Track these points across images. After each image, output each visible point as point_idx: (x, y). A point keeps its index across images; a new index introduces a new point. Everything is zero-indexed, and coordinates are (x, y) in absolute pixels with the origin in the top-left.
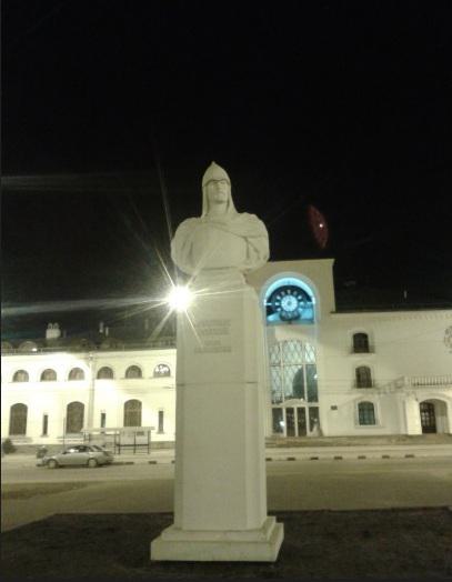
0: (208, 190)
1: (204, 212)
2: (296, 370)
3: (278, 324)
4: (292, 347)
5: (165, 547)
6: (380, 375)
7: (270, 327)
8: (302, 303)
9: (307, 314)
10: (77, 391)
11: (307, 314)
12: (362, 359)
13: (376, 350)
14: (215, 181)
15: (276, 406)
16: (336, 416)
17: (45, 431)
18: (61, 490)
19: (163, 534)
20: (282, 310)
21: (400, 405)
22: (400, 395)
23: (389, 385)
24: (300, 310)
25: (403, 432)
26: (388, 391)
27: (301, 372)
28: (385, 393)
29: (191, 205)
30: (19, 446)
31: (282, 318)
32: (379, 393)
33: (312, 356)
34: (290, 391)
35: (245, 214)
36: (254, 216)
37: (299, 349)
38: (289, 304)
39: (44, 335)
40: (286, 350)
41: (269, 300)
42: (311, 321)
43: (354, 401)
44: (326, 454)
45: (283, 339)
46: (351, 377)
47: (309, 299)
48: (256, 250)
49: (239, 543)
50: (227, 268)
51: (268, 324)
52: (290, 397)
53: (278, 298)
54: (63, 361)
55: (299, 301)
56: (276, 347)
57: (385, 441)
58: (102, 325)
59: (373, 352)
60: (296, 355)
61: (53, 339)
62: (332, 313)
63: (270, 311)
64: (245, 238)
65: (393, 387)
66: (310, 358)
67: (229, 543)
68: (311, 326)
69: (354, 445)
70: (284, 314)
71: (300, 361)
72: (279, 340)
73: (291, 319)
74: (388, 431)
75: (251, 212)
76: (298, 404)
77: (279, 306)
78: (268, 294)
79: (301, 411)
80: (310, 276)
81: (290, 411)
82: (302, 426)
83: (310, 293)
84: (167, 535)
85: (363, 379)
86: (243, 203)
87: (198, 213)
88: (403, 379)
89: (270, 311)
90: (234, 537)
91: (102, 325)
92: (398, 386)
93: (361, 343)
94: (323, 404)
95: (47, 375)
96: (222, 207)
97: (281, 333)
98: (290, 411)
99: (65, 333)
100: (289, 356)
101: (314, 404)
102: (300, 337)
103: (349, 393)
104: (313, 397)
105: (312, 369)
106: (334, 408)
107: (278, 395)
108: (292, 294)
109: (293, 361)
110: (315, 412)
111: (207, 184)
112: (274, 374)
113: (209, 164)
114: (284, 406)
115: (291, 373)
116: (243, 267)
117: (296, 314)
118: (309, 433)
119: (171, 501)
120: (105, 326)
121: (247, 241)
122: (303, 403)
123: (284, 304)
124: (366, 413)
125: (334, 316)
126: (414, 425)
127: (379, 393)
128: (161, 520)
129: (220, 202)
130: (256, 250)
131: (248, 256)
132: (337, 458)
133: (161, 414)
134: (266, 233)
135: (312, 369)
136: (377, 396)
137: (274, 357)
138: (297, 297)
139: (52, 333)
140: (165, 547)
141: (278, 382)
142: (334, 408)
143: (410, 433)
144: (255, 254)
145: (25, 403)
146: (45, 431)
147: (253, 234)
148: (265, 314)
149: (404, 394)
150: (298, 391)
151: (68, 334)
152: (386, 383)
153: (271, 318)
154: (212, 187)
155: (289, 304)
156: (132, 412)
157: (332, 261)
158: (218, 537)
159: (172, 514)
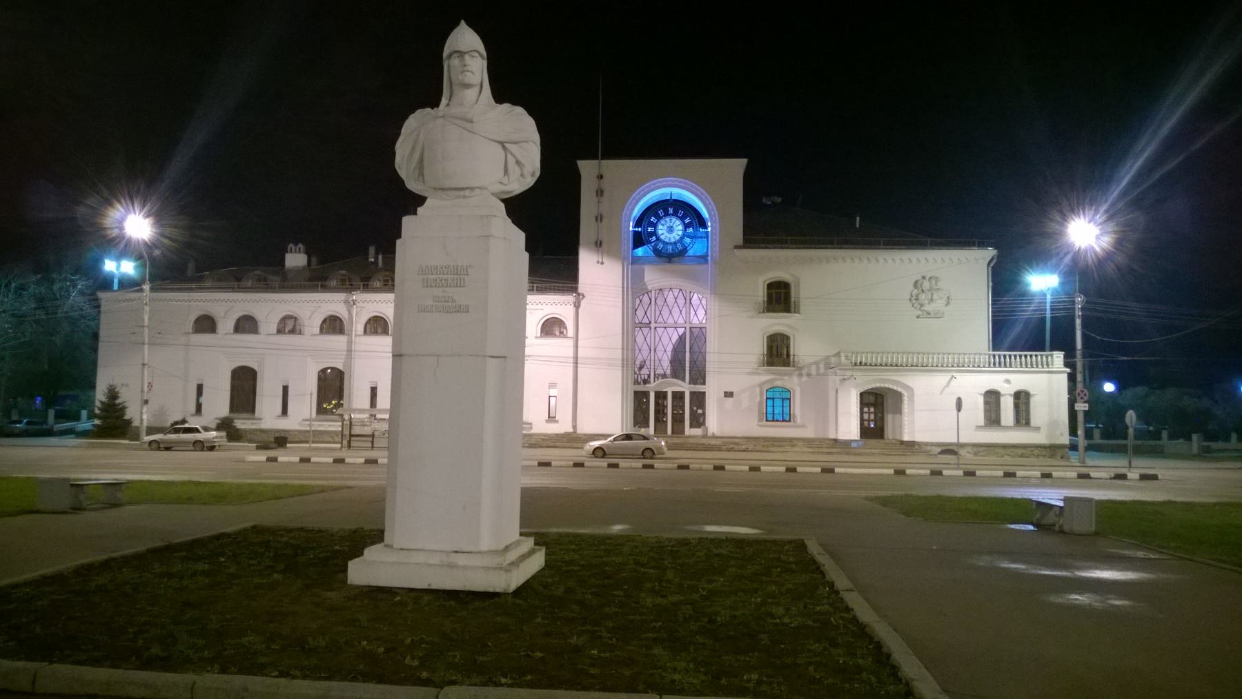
0: (451, 66)
1: (444, 101)
2: (675, 338)
3: (651, 263)
4: (670, 299)
5: (367, 570)
6: (804, 349)
7: (636, 267)
8: (690, 230)
9: (696, 248)
10: (332, 350)
11: (696, 248)
12: (778, 323)
13: (802, 308)
14: (461, 54)
15: (641, 388)
16: (731, 410)
17: (285, 411)
18: (323, 491)
19: (366, 551)
20: (658, 239)
21: (832, 394)
22: (833, 380)
23: (817, 363)
24: (687, 240)
25: (832, 436)
26: (814, 372)
27: (682, 339)
28: (809, 375)
29: (429, 92)
30: (245, 431)
31: (658, 253)
32: (800, 375)
33: (701, 313)
34: (666, 365)
35: (506, 106)
36: (520, 110)
37: (681, 301)
38: (671, 230)
39: (282, 261)
40: (660, 302)
41: (638, 223)
42: (703, 258)
43: (761, 385)
44: (702, 462)
45: (657, 286)
46: (758, 348)
47: (702, 223)
48: (518, 162)
49: (465, 567)
50: (472, 189)
51: (636, 260)
52: (664, 376)
53: (671, 211)
54: (314, 306)
55: (686, 226)
56: (646, 298)
57: (1002, 451)
58: (372, 250)
59: (797, 311)
60: (676, 310)
61: (298, 271)
62: (737, 247)
63: (638, 241)
64: (502, 144)
65: (822, 366)
66: (699, 317)
67: (452, 566)
68: (704, 266)
69: (868, 454)
70: (661, 246)
71: (681, 321)
72: (649, 287)
73: (670, 256)
74: (809, 433)
75: (515, 103)
76: (672, 387)
77: (654, 234)
78: (637, 212)
79: (678, 396)
80: (709, 188)
81: (661, 396)
82: (678, 420)
83: (705, 214)
84: (371, 553)
85: (777, 352)
86: (504, 88)
87: (435, 103)
88: (838, 354)
89: (638, 241)
90: (461, 560)
91: (372, 250)
92: (829, 365)
93: (779, 297)
94: (713, 389)
95: (289, 325)
96: (471, 94)
97: (653, 277)
98: (661, 396)
99: (314, 260)
100: (665, 312)
101: (699, 388)
102: (687, 285)
103: (758, 374)
104: (699, 376)
105: (698, 335)
106: (729, 395)
107: (645, 371)
108: (675, 214)
109: (671, 321)
110: (699, 399)
111: (450, 56)
112: (640, 339)
113: (457, 24)
114: (652, 387)
115: (668, 340)
116: (498, 188)
117: (679, 246)
118: (688, 431)
119: (381, 513)
120: (377, 254)
121: (504, 148)
122: (686, 387)
123: (662, 230)
124: (777, 406)
125: (738, 252)
126: (849, 426)
127: (800, 375)
128: (369, 535)
129: (468, 86)
130: (518, 162)
131: (506, 171)
132: (717, 468)
133: (374, 391)
134: (536, 137)
135: (698, 335)
136: (795, 379)
137: (640, 313)
138: (682, 219)
139: (295, 259)
140: (367, 570)
141: (645, 352)
142: (729, 395)
143: (842, 436)
144: (517, 168)
145: (256, 368)
146: (285, 411)
147: (515, 137)
148: (631, 246)
149: (838, 378)
150: (677, 370)
151: (321, 262)
152: (811, 360)
153: (640, 251)
154: (455, 62)
155: (671, 230)
156: (332, 387)
157: (744, 161)
158: (435, 560)
159: (382, 532)
